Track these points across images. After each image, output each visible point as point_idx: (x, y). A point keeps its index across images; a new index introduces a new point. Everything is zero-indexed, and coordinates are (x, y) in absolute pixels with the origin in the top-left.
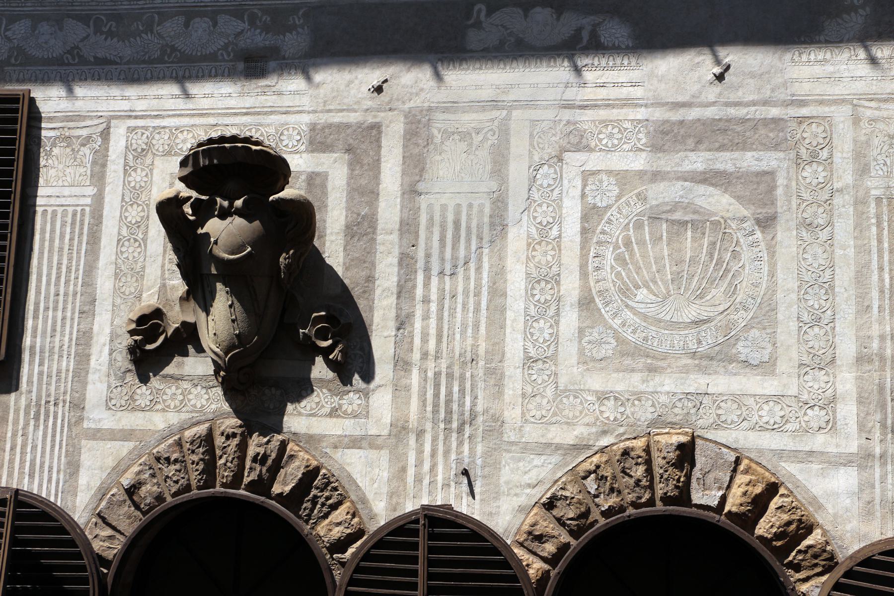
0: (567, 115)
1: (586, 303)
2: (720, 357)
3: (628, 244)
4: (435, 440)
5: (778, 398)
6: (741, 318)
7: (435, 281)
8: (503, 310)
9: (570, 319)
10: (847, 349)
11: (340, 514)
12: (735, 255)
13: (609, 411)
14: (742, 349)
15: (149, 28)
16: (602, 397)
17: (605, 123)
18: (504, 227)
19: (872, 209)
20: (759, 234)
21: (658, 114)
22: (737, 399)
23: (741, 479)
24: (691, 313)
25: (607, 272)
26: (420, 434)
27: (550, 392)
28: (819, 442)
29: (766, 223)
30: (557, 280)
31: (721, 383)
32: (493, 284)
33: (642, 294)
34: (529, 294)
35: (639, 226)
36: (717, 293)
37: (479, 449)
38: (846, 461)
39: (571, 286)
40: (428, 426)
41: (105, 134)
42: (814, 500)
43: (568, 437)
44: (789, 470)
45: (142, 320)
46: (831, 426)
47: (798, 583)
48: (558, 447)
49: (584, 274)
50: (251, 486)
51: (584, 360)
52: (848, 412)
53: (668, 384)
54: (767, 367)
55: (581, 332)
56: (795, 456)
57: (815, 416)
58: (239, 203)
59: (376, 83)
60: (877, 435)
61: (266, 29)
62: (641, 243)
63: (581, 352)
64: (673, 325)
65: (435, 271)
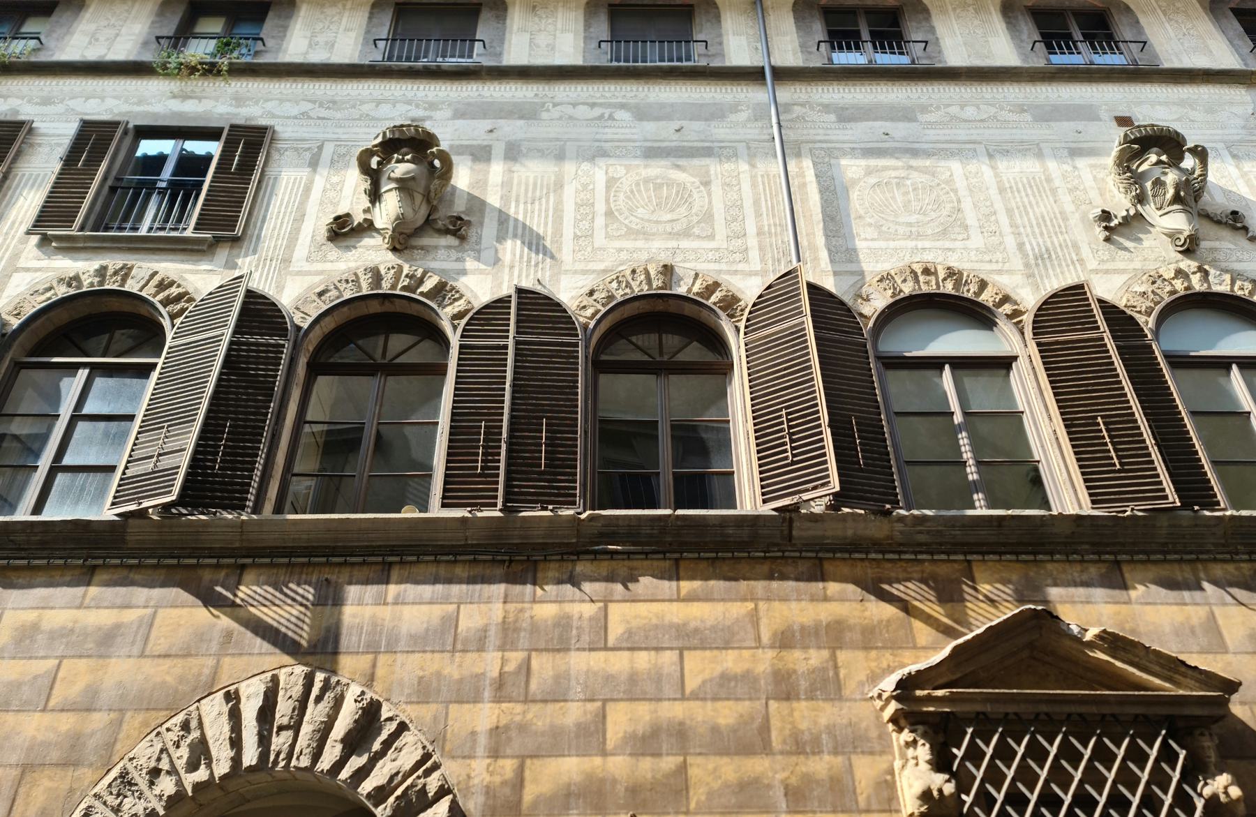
0: (597, 144)
1: (609, 214)
2: (686, 233)
3: (632, 192)
4: (521, 270)
5: (717, 250)
6: (695, 219)
7: (522, 206)
8: (561, 218)
9: (600, 221)
10: (751, 228)
11: (462, 302)
12: (690, 195)
13: (624, 255)
14: (696, 231)
15: (354, 107)
16: (620, 250)
17: (618, 147)
18: (562, 186)
19: (760, 179)
20: (702, 188)
21: (325, 427)
22: (695, 251)
23: (699, 282)
24: (669, 217)
25: (620, 202)
26: (512, 267)
27: (589, 249)
28: (741, 267)
29: (707, 184)
30: (593, 205)
31: (685, 244)
32: (555, 210)
33: (641, 210)
34: (577, 210)
35: (638, 184)
36: (683, 210)
37: (548, 274)
38: (756, 274)
39: (600, 207)
40: (517, 264)
41: (320, 148)
42: (739, 289)
43: (602, 266)
44: (722, 278)
45: (337, 218)
46: (745, 260)
47: (15, 444)
48: (594, 271)
49: (607, 201)
50: (404, 288)
51: (608, 236)
52: (754, 254)
53: (656, 245)
54: (711, 237)
55: (607, 226)
56: (728, 272)
57: (738, 256)
58: (409, 157)
59: (489, 128)
60: (770, 262)
61: (425, 109)
62: (639, 191)
63: (607, 233)
64: (657, 222)
65: (522, 200)
